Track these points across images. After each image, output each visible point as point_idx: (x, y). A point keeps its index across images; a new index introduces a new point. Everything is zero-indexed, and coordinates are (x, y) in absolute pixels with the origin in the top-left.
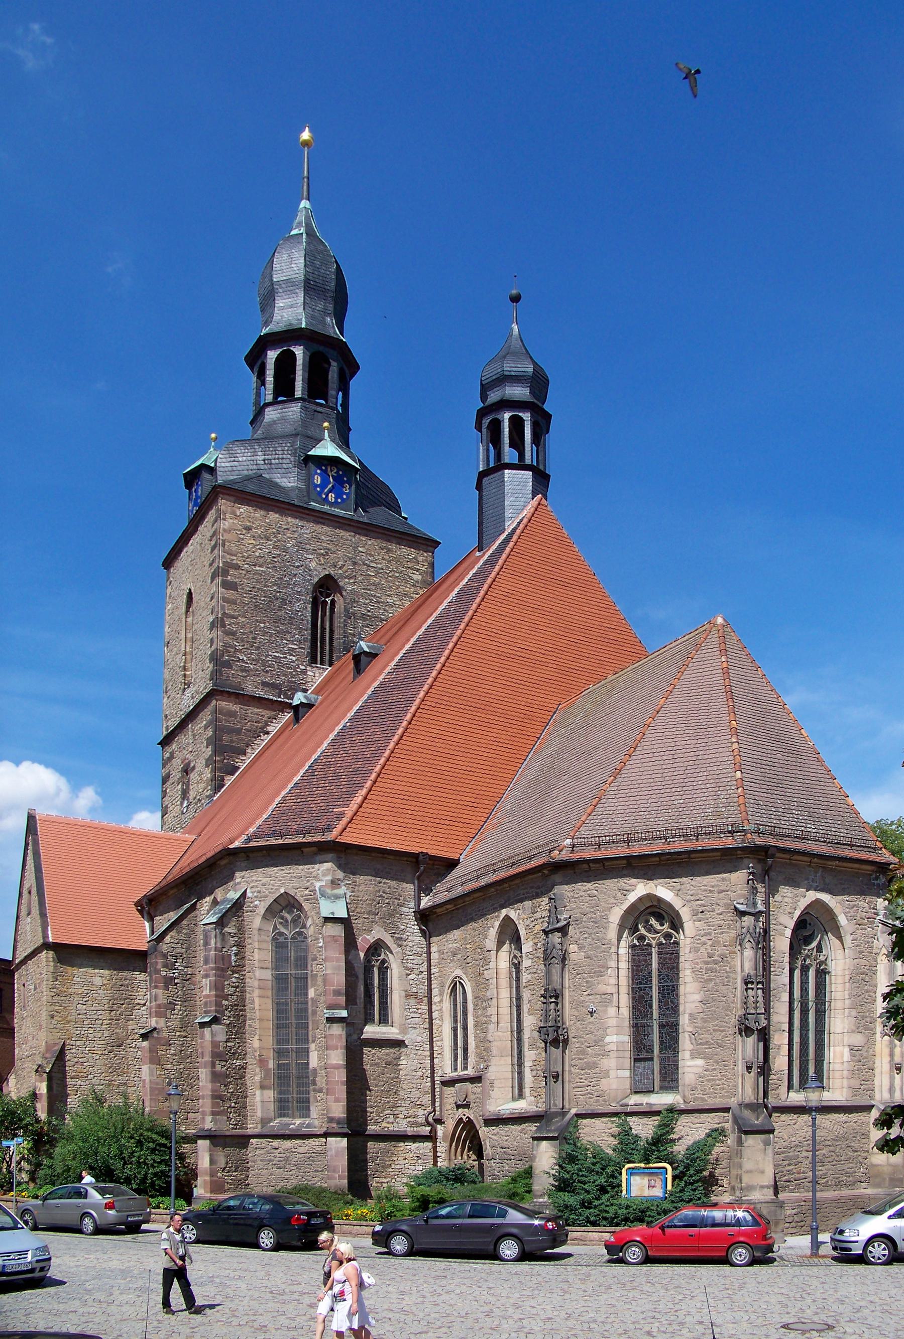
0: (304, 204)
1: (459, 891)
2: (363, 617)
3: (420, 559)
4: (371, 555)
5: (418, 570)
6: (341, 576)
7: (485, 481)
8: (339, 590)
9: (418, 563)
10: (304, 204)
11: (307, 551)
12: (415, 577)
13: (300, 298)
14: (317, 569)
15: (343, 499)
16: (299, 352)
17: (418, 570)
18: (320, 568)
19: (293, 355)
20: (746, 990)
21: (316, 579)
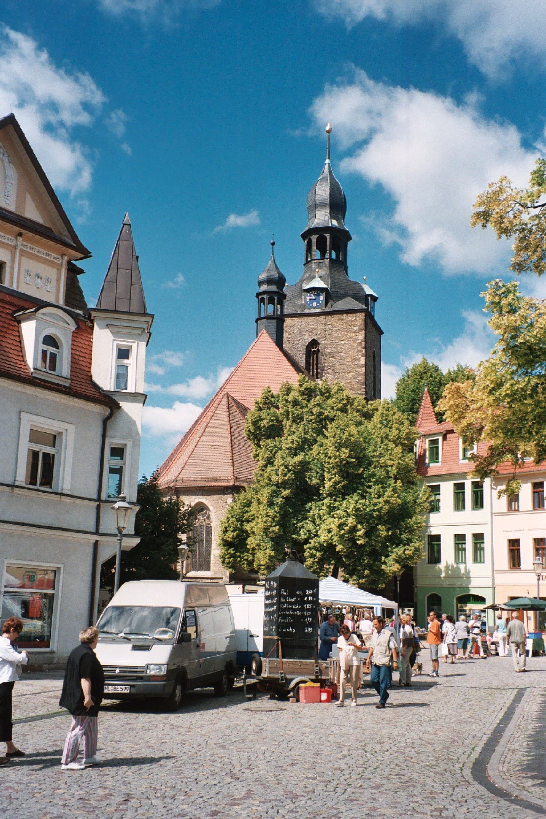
0: (327, 161)
1: (30, 766)
2: (330, 354)
3: (358, 319)
4: (334, 325)
5: (357, 325)
6: (320, 338)
7: (259, 321)
8: (318, 344)
9: (357, 321)
10: (327, 161)
11: (303, 331)
12: (355, 328)
13: (328, 211)
14: (308, 339)
15: (320, 304)
16: (328, 236)
17: (357, 325)
18: (309, 338)
19: (326, 238)
20: (496, 650)
21: (307, 343)
